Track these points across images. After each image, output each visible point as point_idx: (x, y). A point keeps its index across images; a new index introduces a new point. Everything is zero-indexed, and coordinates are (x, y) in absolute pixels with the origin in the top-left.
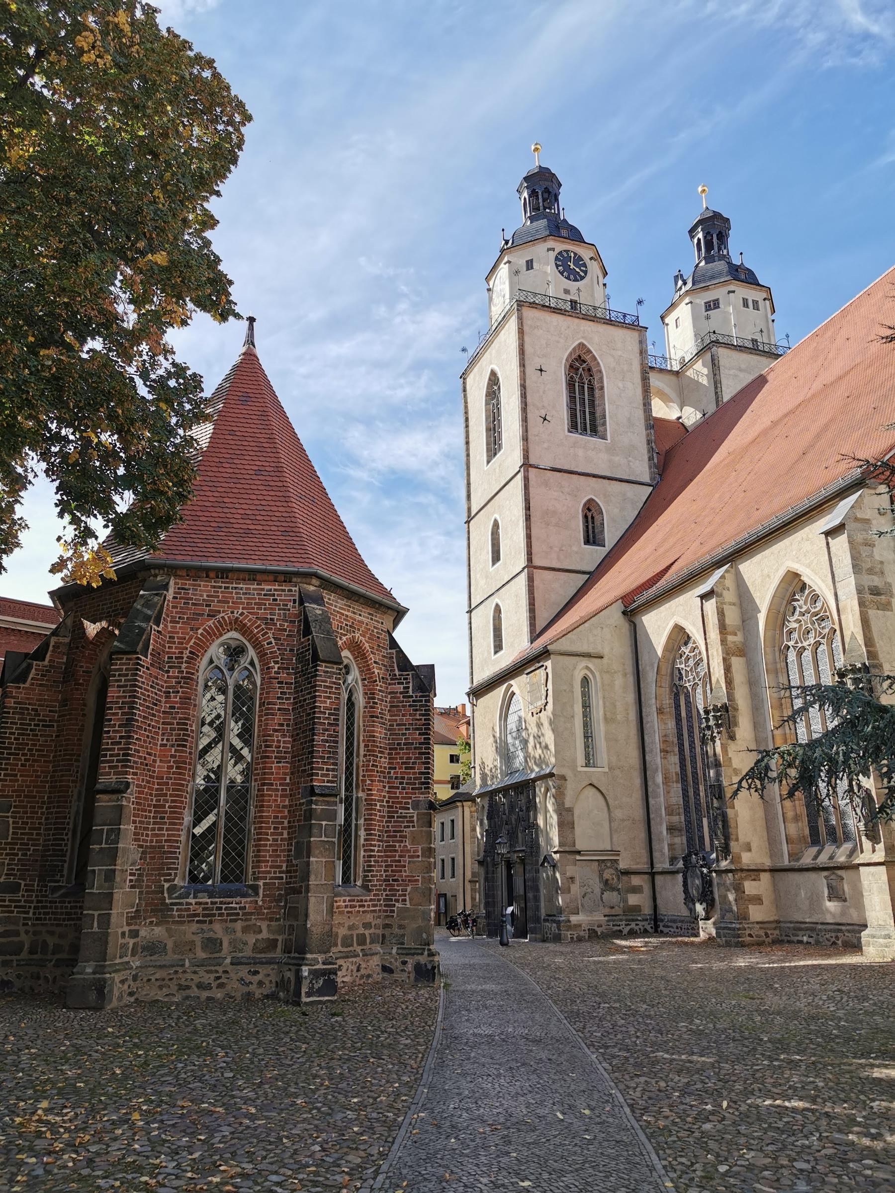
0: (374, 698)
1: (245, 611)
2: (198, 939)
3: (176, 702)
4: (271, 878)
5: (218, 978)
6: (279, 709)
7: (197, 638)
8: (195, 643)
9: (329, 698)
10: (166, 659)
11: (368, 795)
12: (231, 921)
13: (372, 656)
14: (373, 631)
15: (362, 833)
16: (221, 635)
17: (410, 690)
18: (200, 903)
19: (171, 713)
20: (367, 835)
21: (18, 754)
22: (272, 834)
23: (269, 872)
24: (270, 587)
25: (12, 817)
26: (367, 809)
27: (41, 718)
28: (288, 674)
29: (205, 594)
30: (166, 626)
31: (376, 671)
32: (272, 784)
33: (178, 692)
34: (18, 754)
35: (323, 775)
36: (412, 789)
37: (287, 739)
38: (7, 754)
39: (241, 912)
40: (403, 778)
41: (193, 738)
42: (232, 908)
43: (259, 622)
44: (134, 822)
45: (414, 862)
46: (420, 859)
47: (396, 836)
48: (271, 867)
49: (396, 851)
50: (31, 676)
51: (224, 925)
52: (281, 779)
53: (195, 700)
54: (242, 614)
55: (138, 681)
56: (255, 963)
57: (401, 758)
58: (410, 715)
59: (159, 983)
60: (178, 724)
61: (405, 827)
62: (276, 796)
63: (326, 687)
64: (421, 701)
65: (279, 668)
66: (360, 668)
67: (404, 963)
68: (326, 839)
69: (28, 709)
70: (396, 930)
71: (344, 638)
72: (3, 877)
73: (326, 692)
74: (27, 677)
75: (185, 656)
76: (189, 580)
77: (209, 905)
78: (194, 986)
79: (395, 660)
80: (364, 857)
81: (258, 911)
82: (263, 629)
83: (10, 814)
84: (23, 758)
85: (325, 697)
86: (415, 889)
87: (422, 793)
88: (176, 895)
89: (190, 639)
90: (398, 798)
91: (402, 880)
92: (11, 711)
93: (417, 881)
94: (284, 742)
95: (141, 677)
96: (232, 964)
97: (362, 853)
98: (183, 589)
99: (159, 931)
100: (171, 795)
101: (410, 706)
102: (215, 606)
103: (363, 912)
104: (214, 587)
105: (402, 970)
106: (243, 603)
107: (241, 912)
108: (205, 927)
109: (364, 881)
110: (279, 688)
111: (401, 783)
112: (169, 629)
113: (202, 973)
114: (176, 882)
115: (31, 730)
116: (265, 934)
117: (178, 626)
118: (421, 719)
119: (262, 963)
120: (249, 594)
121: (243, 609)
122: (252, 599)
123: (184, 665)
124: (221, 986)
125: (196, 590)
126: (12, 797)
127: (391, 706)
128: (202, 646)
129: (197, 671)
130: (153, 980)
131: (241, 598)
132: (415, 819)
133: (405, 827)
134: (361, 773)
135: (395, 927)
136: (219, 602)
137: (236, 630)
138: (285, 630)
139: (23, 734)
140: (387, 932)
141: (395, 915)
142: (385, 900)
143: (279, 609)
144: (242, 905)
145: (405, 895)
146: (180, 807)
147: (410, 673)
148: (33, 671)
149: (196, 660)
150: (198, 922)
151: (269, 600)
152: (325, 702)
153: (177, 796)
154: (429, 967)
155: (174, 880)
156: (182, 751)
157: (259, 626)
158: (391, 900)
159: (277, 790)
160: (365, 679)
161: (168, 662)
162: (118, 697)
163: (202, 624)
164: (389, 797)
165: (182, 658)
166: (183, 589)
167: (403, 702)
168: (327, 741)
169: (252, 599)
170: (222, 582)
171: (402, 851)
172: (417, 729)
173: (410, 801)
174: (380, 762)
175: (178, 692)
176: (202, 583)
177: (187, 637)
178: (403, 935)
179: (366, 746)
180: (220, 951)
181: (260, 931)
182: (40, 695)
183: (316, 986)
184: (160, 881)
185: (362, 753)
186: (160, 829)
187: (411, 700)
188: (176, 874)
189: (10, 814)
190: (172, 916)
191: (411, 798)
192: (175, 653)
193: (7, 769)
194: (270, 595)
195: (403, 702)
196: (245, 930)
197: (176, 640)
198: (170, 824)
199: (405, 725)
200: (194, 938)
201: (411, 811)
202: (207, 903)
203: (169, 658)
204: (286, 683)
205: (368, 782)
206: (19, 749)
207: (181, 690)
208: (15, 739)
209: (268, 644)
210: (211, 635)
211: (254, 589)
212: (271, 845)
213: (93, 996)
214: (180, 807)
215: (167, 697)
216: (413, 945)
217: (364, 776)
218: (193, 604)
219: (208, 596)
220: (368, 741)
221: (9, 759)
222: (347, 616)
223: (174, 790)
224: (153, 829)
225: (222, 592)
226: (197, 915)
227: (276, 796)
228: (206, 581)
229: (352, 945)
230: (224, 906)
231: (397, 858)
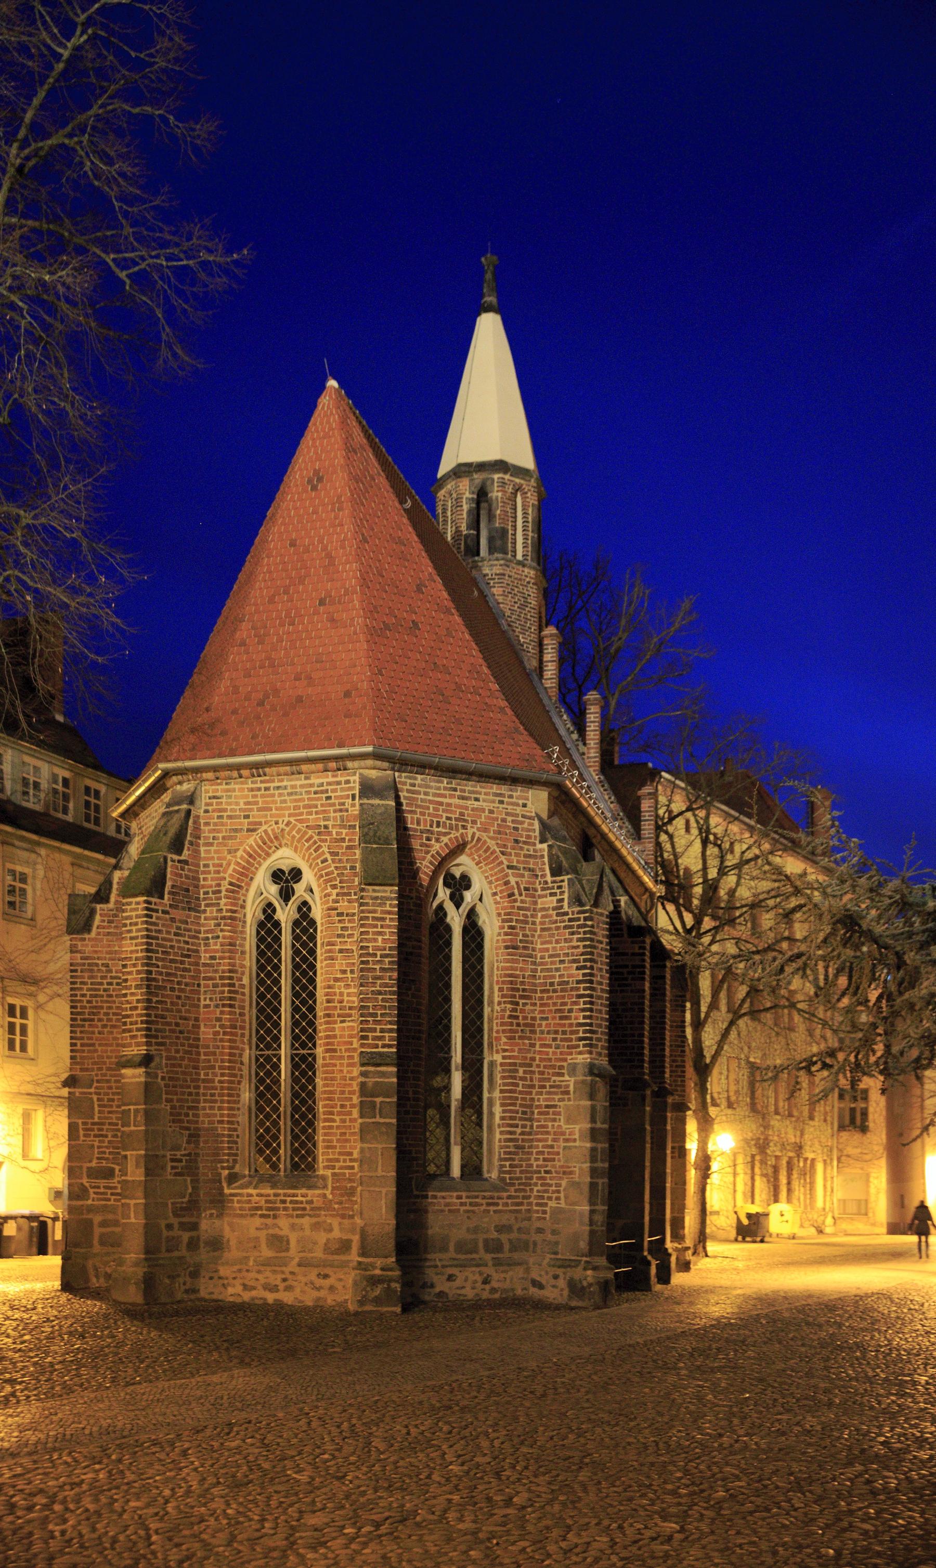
1: (292, 819)
2: (263, 1235)
3: (216, 951)
5: (284, 1280)
6: (341, 951)
8: (234, 870)
9: (380, 933)
12: (297, 1216)
14: (504, 820)
16: (268, 855)
17: (566, 904)
18: (262, 1195)
24: (321, 781)
25: (96, 1093)
27: (114, 974)
28: (350, 901)
33: (218, 937)
34: (93, 1020)
35: (375, 1038)
36: (568, 1047)
37: (352, 990)
38: (82, 1020)
39: (308, 1207)
41: (243, 994)
42: (297, 1202)
43: (310, 832)
44: (167, 1100)
45: (570, 1148)
47: (548, 1113)
48: (340, 1154)
51: (291, 1220)
54: (288, 824)
56: (324, 1266)
57: (555, 1004)
61: (559, 1100)
63: (374, 919)
64: (579, 919)
68: (382, 1120)
69: (97, 965)
70: (550, 1237)
71: (445, 839)
72: (95, 1161)
73: (376, 926)
75: (223, 889)
77: (272, 1198)
78: (260, 1287)
79: (546, 860)
80: (500, 1141)
81: (328, 1205)
82: (315, 842)
83: (92, 1090)
84: (99, 1024)
89: (229, 864)
90: (550, 1060)
92: (79, 968)
94: (349, 995)
96: (299, 1265)
97: (498, 1136)
98: (214, 797)
101: (565, 927)
102: (255, 816)
103: (495, 1212)
104: (252, 790)
106: (289, 808)
107: (308, 1207)
108: (269, 1221)
110: (340, 921)
111: (554, 1039)
113: (268, 1274)
115: (105, 990)
116: (336, 1234)
117: (212, 848)
118: (578, 947)
119: (332, 1266)
120: (296, 793)
121: (290, 815)
122: (300, 800)
123: (223, 901)
126: (93, 1070)
127: (543, 930)
129: (243, 907)
132: (571, 1088)
134: (495, 1028)
136: (259, 810)
138: (343, 840)
139: (96, 996)
141: (547, 1216)
143: (335, 811)
145: (558, 1192)
147: (566, 878)
148: (98, 918)
150: (262, 1216)
151: (321, 799)
152: (375, 940)
155: (233, 1168)
157: (311, 837)
160: (495, 894)
161: (205, 899)
162: (132, 952)
163: (241, 844)
166: (214, 797)
167: (556, 922)
168: (380, 993)
169: (300, 800)
170: (261, 782)
172: (574, 961)
173: (565, 1064)
175: (218, 937)
176: (237, 787)
177: (224, 863)
178: (557, 1243)
180: (287, 1250)
181: (331, 1230)
182: (109, 946)
184: (216, 1169)
187: (566, 918)
191: (565, 1060)
192: (211, 886)
194: (322, 792)
195: (556, 922)
196: (316, 1227)
200: (259, 1234)
201: (567, 1078)
202: (269, 1195)
206: (94, 1014)
207: (221, 934)
209: (323, 862)
211: (302, 786)
215: (206, 945)
217: (498, 1032)
218: (230, 817)
222: (449, 805)
225: (262, 796)
226: (260, 1208)
229: (477, 1252)
230: (289, 1199)
231: (550, 1143)
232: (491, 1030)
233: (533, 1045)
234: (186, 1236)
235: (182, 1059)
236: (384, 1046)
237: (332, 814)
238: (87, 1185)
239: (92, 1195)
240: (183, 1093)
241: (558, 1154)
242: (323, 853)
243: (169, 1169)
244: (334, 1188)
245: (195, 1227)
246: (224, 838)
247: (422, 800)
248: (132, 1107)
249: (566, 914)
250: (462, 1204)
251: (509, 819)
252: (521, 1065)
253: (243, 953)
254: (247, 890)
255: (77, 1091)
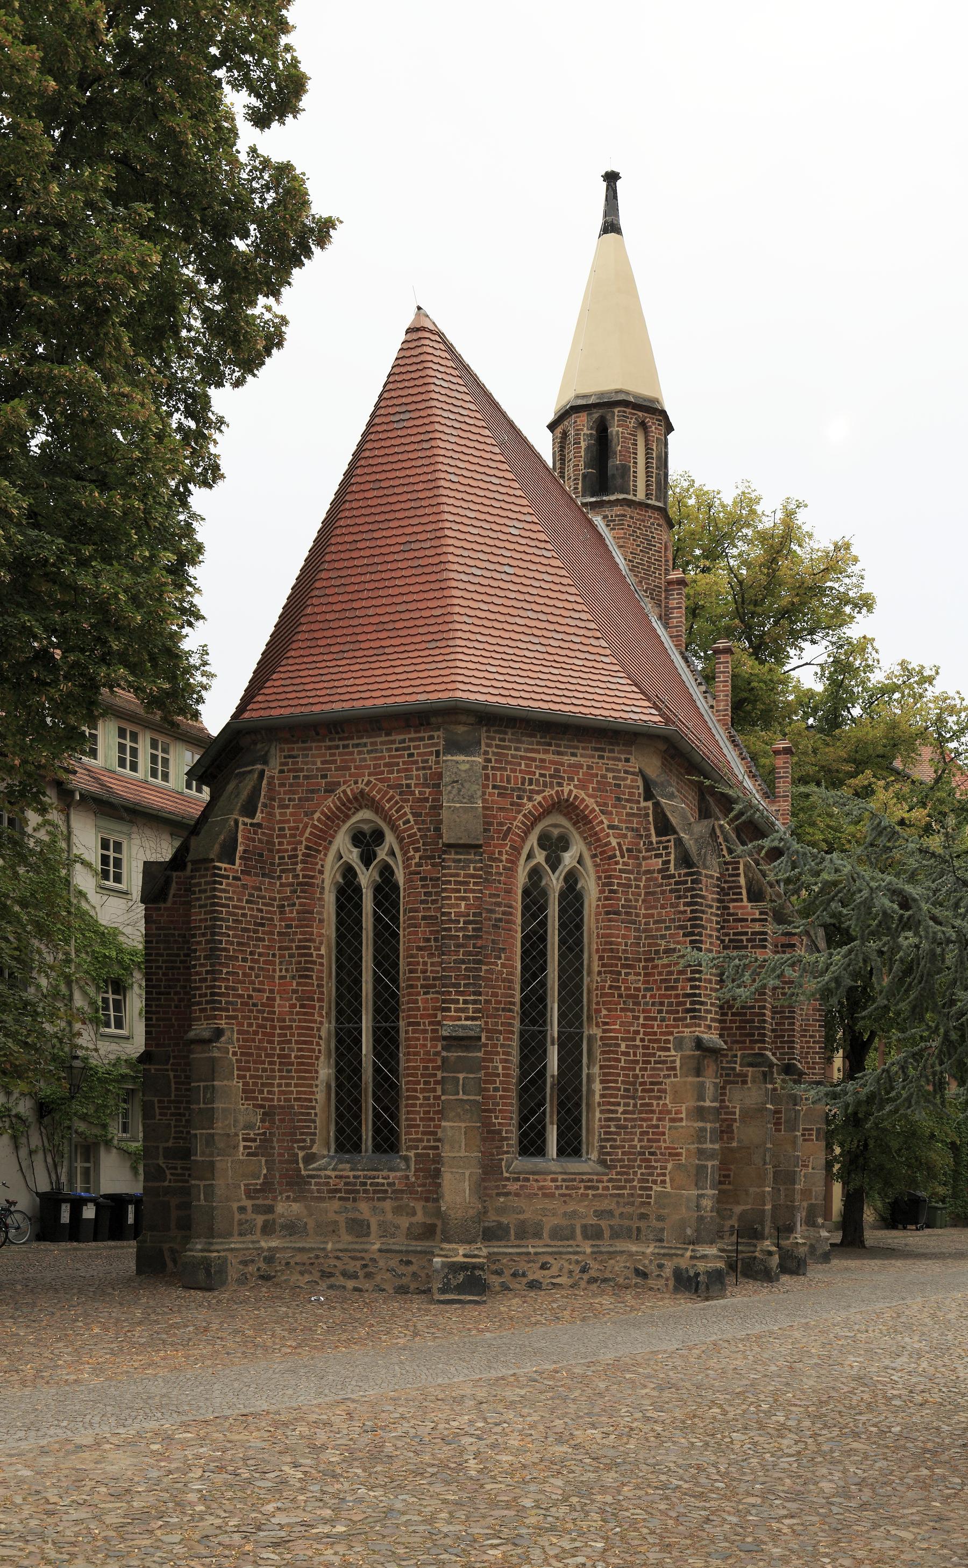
0: (612, 884)
1: (372, 779)
2: (341, 1219)
3: (292, 919)
4: (424, 1148)
5: (365, 1266)
6: (424, 918)
7: (314, 827)
9: (463, 899)
10: (277, 861)
11: (605, 1031)
12: (379, 1199)
13: (603, 817)
15: (597, 1087)
18: (341, 1177)
19: (287, 934)
20: (604, 1089)
21: (169, 993)
22: (423, 1090)
23: (421, 1140)
25: (172, 1070)
26: (603, 1052)
28: (433, 865)
29: (319, 761)
30: (271, 814)
31: (614, 843)
32: (418, 1024)
34: (169, 993)
36: (675, 1019)
40: (662, 1004)
41: (322, 964)
42: (378, 1184)
44: (239, 1077)
45: (676, 1128)
46: (684, 1124)
47: (653, 1090)
48: (424, 1133)
49: (653, 1112)
50: (172, 892)
52: (430, 1016)
53: (320, 913)
54: (369, 782)
55: (221, 898)
57: (660, 974)
58: (672, 906)
59: (299, 1268)
60: (298, 948)
61: (665, 1076)
62: (425, 1039)
63: (457, 883)
65: (420, 858)
66: (585, 839)
67: (660, 1266)
68: (465, 1097)
70: (654, 1223)
71: (539, 798)
73: (459, 891)
74: (167, 894)
75: (300, 853)
76: (297, 742)
77: (352, 1180)
79: (651, 819)
80: (600, 1120)
82: (397, 803)
83: (169, 1067)
85: (457, 898)
86: (679, 1167)
87: (687, 1026)
88: (314, 1165)
89: (306, 827)
90: (655, 1034)
91: (661, 1154)
93: (679, 1154)
94: (433, 964)
95: (225, 891)
97: (598, 1115)
98: (290, 757)
99: (296, 1207)
100: (297, 1042)
101: (671, 891)
105: (659, 1276)
106: (368, 767)
108: (349, 1205)
109: (601, 1153)
110: (423, 886)
111: (660, 1012)
112: (278, 818)
114: (314, 1150)
115: (181, 962)
116: (420, 1218)
117: (288, 811)
118: (685, 911)
123: (299, 867)
124: (368, 1276)
125: (307, 756)
127: (647, 894)
128: (324, 837)
129: (321, 872)
130: (292, 1263)
131: (365, 760)
132: (678, 1064)
133: (665, 1076)
134: (595, 1000)
135: (653, 1217)
137: (367, 807)
138: (426, 800)
139: (173, 968)
140: (642, 1224)
141: (652, 1201)
142: (640, 1181)
143: (417, 769)
144: (391, 1180)
146: (310, 1057)
148: (174, 885)
149: (315, 857)
150: (341, 1199)
152: (458, 906)
153: (305, 1042)
154: (692, 1273)
155: (311, 1147)
156: (306, 984)
158: (647, 1181)
159: (425, 1031)
161: (280, 865)
163: (318, 805)
164: (645, 1034)
165: (296, 856)
167: (662, 885)
168: (463, 962)
171: (660, 1112)
172: (681, 927)
173: (671, 1038)
174: (625, 981)
175: (294, 905)
176: (314, 745)
177: (301, 826)
178: (663, 1229)
179: (601, 958)
180: (368, 1234)
183: (454, 1283)
184: (293, 1148)
185: (596, 969)
186: (288, 1085)
188: (313, 1141)
189: (169, 1067)
190: (311, 1191)
191: (671, 1033)
192: (287, 851)
193: (158, 1012)
195: (662, 885)
197: (287, 832)
198: (299, 1078)
199: (664, 921)
201: (673, 1053)
202: (348, 1177)
203: (280, 858)
204: (431, 880)
205: (604, 1012)
208: (164, 974)
210: (334, 820)
212: (421, 1105)
213: (201, 1276)
214: (310, 1057)
215: (281, 913)
216: (674, 1243)
217: (598, 1003)
218: (306, 777)
219: (323, 763)
220: (604, 950)
221: (159, 999)
222: (542, 761)
223: (299, 1035)
224: (280, 1085)
226: (339, 1191)
227: (425, 1039)
228: (319, 741)
230: (369, 1181)
231: (654, 1122)
232: (589, 1001)
233: (637, 1018)
234: (260, 1220)
235: (256, 1033)
236: (467, 1019)
237: (415, 773)
238: (164, 1166)
239: (169, 1177)
240: (257, 1070)
241: (664, 1134)
242: (405, 814)
243: (241, 1149)
244: (416, 1170)
245: (270, 1209)
246: (300, 799)
247: (513, 756)
248: (202, 1084)
249: (673, 876)
250: (557, 1188)
251: (610, 775)
252: (623, 1039)
253: (321, 921)
254: (326, 855)
255: (153, 1068)
